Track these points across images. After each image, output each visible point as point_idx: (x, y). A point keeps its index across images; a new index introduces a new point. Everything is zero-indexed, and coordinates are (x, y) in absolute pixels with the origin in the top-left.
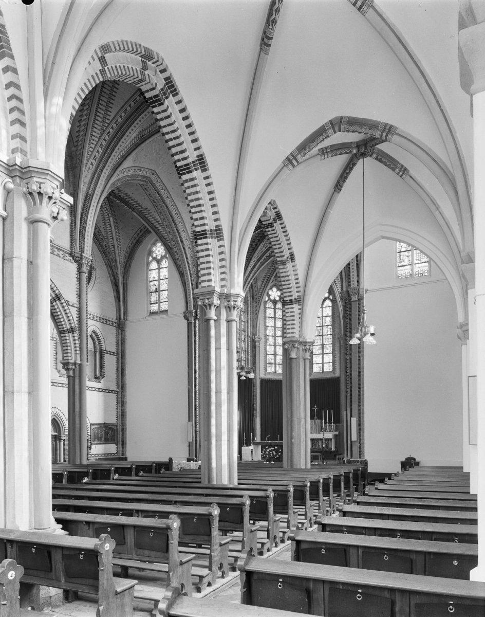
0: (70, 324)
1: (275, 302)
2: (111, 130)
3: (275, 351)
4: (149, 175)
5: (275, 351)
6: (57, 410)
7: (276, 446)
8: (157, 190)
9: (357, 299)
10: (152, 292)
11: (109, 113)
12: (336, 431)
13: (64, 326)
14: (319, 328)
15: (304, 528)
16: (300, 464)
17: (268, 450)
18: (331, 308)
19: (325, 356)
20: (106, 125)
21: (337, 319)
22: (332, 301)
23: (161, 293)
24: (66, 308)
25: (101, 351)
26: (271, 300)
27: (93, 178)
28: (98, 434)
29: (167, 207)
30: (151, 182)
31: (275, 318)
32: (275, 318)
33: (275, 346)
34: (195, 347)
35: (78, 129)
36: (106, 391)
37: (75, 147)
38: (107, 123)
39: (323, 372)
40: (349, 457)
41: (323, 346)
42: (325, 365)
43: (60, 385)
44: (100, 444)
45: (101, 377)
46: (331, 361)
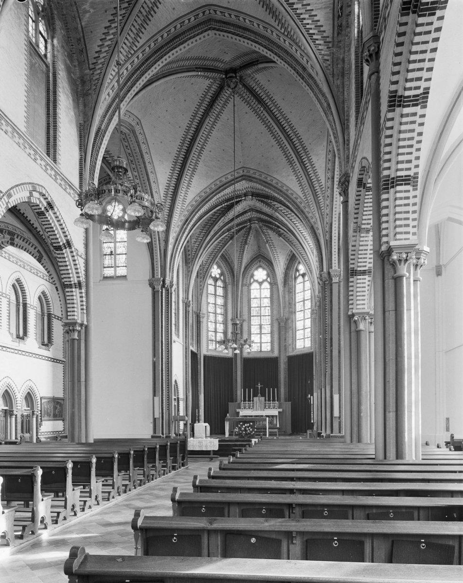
0: (78, 277)
1: (216, 280)
2: (136, 60)
3: (216, 329)
4: (133, 124)
5: (216, 329)
6: (10, 380)
7: (252, 422)
8: (138, 142)
9: (337, 281)
10: (106, 255)
11: (138, 39)
12: (279, 408)
13: (72, 279)
14: (257, 309)
15: (111, 497)
16: (82, 440)
17: (244, 426)
18: (269, 290)
19: (262, 335)
20: (133, 52)
21: (275, 301)
22: (270, 283)
23: (117, 257)
24: (76, 258)
25: (49, 315)
26: (212, 277)
27: (107, 111)
28: (48, 409)
29: (144, 163)
30: (134, 132)
31: (215, 295)
32: (215, 295)
33: (216, 323)
34: (162, 315)
35: (98, 49)
36: (55, 360)
37: (90, 70)
38: (134, 50)
39: (261, 351)
40: (328, 432)
41: (261, 326)
42: (263, 345)
43: (13, 351)
44: (49, 420)
45: (50, 345)
46: (270, 341)
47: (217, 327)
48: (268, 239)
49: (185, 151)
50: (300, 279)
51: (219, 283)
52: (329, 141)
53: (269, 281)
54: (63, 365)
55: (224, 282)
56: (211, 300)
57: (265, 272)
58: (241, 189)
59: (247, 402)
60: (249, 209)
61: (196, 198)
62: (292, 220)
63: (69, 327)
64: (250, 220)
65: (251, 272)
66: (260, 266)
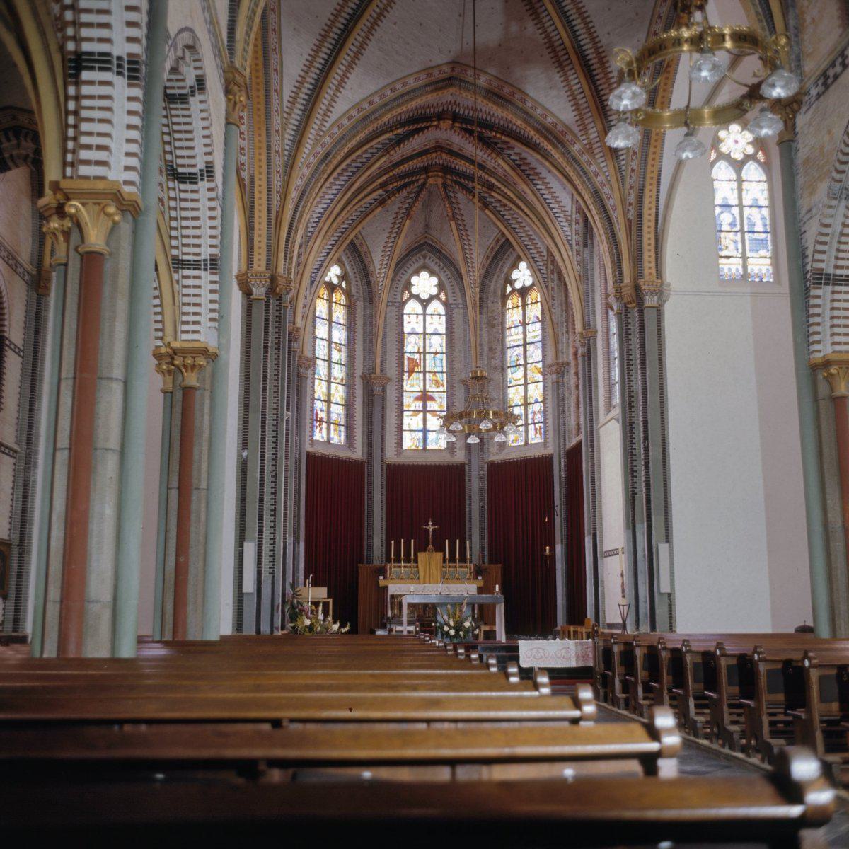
5: (329, 395)
9: (656, 305)
18: (443, 319)
33: (329, 382)
47: (333, 391)
48: (456, 211)
49: (348, 17)
50: (515, 300)
51: (339, 297)
52: (652, 32)
53: (444, 299)
54: (13, 461)
55: (348, 293)
56: (321, 331)
57: (435, 280)
58: (435, 105)
59: (402, 564)
60: (435, 147)
61: (350, 113)
62: (531, 177)
63: (184, 357)
64: (426, 169)
65: (405, 277)
66: (425, 268)
